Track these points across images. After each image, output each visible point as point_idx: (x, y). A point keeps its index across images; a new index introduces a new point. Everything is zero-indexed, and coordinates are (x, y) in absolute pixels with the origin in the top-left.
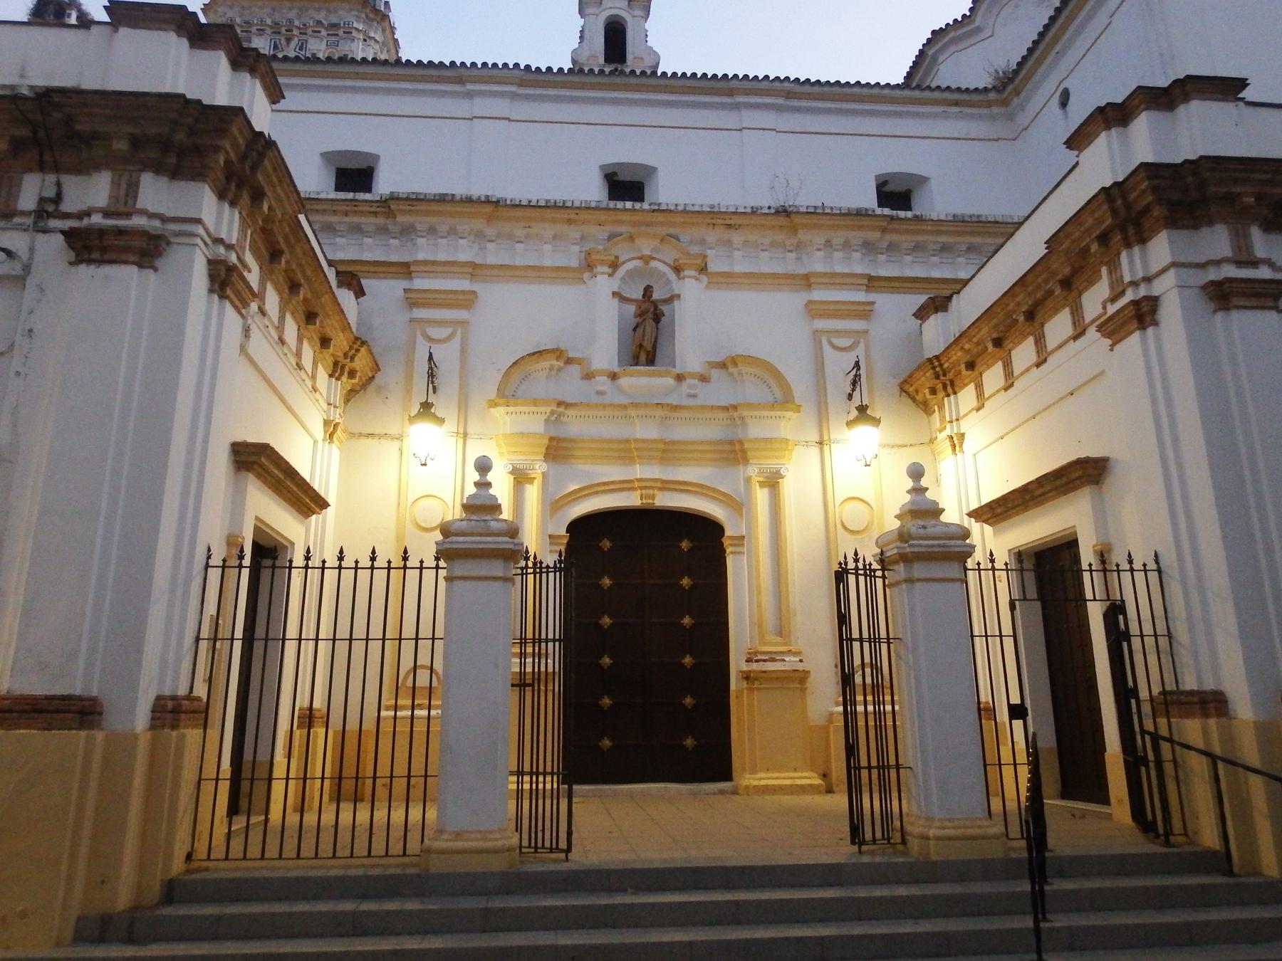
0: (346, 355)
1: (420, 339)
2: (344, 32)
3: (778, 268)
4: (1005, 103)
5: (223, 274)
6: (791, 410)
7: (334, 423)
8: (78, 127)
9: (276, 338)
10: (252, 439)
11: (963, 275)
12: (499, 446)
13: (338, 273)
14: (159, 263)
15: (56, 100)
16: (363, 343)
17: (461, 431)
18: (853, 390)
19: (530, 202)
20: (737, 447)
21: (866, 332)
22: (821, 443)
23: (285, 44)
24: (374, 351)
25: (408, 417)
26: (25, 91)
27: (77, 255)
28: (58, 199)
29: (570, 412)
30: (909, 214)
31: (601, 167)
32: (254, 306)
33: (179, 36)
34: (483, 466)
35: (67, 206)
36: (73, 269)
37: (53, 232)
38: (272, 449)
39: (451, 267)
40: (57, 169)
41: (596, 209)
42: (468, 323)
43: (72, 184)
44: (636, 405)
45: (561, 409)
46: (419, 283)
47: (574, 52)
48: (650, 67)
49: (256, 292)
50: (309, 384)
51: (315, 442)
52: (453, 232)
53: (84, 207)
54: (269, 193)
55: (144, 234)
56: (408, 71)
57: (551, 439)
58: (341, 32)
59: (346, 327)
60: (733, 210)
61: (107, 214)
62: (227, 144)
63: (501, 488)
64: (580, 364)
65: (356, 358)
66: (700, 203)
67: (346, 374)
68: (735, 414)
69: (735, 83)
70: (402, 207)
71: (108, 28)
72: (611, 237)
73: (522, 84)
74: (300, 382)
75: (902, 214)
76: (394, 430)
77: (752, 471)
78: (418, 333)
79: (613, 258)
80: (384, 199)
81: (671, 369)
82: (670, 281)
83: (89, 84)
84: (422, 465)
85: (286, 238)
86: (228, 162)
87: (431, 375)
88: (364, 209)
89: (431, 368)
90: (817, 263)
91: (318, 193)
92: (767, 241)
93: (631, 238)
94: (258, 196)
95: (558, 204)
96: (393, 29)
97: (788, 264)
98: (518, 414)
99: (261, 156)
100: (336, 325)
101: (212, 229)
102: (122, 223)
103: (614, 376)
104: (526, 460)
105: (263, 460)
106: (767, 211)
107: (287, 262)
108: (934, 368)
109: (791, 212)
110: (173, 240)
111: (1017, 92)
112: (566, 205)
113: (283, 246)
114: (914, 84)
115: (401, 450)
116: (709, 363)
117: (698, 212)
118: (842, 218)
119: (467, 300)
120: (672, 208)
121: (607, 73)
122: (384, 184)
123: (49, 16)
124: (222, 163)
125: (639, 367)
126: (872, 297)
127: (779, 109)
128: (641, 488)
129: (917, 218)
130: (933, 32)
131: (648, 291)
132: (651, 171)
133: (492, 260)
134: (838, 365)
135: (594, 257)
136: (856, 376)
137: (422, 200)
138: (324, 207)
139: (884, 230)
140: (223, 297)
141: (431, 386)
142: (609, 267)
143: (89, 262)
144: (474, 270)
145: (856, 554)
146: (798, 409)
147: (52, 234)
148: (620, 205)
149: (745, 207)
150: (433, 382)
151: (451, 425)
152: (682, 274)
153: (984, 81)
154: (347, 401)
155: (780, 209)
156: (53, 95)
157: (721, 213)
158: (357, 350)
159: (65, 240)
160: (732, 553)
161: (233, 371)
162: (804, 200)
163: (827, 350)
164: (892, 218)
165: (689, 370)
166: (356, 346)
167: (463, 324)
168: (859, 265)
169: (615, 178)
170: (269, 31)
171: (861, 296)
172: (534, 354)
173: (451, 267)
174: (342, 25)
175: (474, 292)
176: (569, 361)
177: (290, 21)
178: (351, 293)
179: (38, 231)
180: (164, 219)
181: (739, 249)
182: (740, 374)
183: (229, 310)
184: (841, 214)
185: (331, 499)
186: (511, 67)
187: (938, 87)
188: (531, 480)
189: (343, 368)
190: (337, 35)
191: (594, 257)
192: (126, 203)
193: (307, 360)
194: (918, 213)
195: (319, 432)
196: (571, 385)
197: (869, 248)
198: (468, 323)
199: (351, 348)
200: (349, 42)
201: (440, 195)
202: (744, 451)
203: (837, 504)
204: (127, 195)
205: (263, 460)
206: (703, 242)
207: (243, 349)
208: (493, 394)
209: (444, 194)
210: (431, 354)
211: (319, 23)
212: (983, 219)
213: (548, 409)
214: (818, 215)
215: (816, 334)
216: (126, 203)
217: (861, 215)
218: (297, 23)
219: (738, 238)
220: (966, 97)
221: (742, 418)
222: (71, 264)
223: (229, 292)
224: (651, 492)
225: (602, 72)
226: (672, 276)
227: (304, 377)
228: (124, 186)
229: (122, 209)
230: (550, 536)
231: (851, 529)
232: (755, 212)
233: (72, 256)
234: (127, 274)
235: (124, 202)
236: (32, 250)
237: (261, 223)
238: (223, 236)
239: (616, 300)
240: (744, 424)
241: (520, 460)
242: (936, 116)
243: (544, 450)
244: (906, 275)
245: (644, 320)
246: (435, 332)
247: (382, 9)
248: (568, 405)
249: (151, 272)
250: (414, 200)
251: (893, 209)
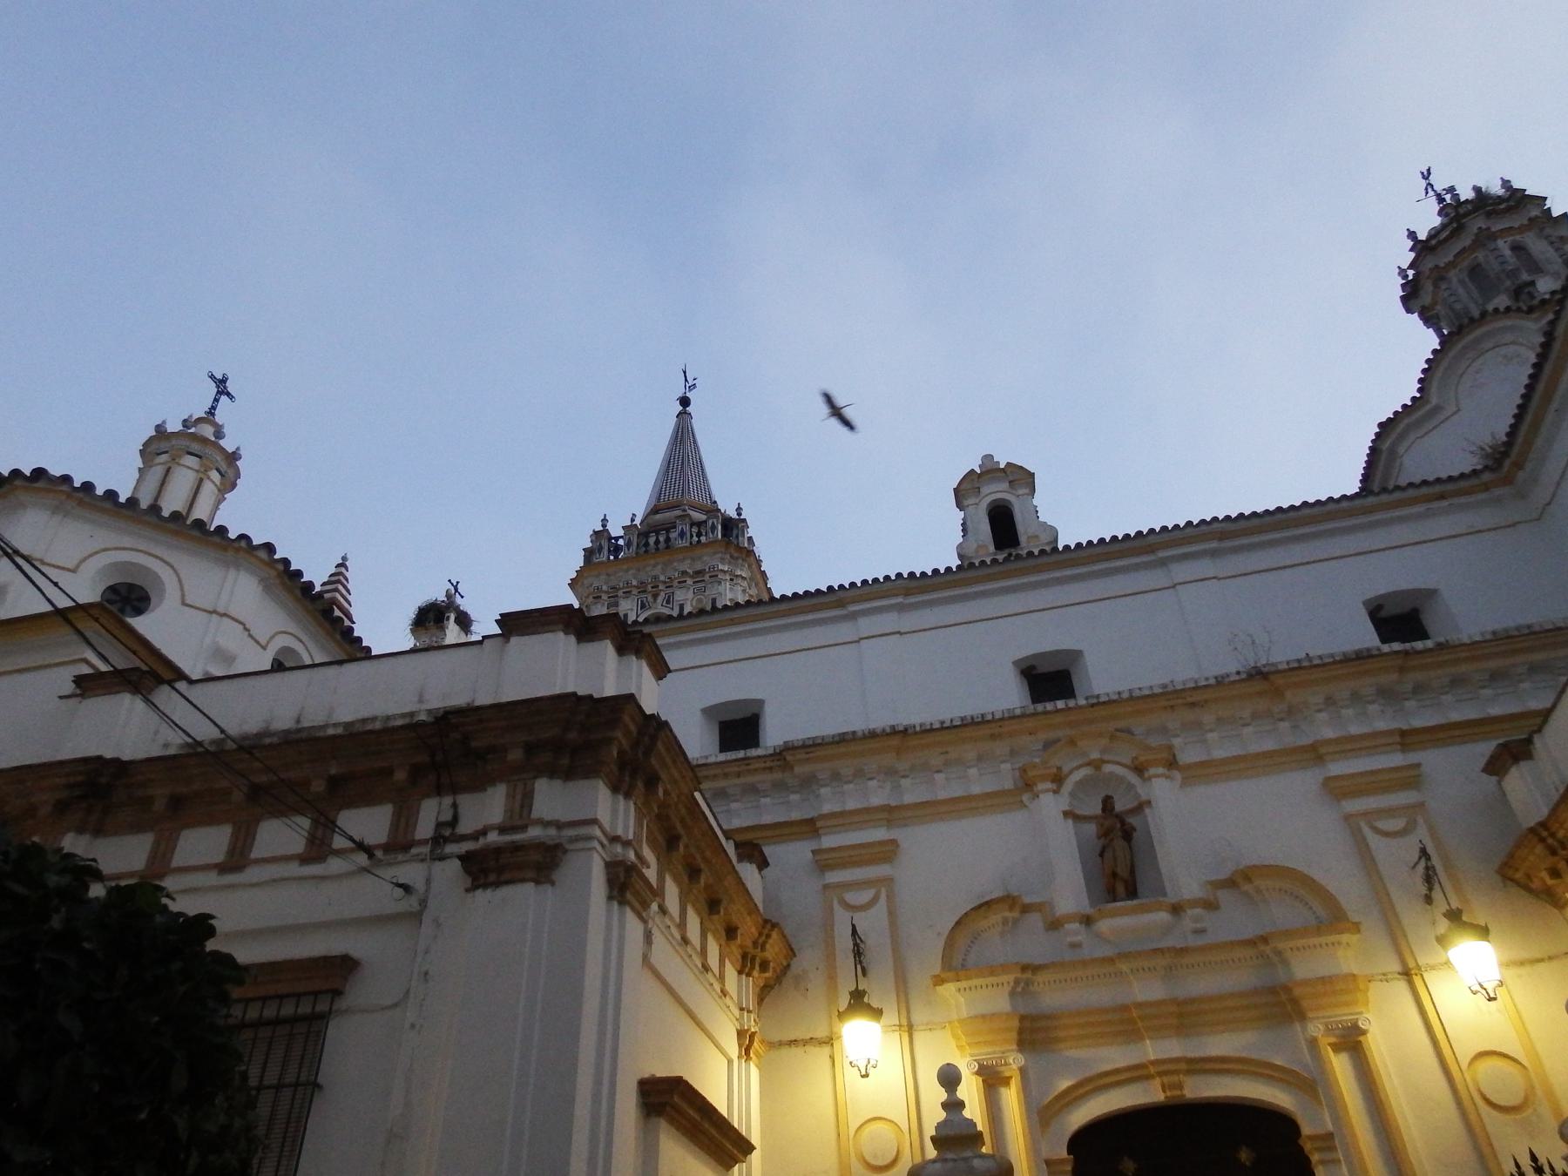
0: (755, 943)
1: (839, 911)
2: (710, 577)
3: (1269, 745)
4: (1508, 481)
5: (622, 875)
6: (1348, 930)
7: (750, 1033)
8: (474, 744)
9: (679, 937)
10: (661, 1072)
11: (1535, 704)
12: (955, 1036)
13: (737, 846)
14: (555, 876)
15: (454, 721)
16: (774, 926)
17: (904, 1022)
18: (1430, 889)
19: (942, 723)
20: (1284, 997)
21: (1422, 805)
22: (1407, 974)
23: (652, 600)
24: (786, 932)
25: (837, 1014)
26: (423, 717)
27: (473, 880)
28: (455, 821)
29: (1041, 978)
30: (1429, 644)
31: (1016, 663)
32: (654, 907)
33: (566, 634)
34: (949, 1078)
35: (464, 828)
36: (471, 895)
37: (449, 858)
38: (687, 1083)
39: (865, 816)
40: (455, 789)
41: (1023, 716)
42: (892, 879)
43: (466, 802)
44: (1124, 956)
45: (1028, 975)
46: (828, 841)
47: (960, 547)
48: (1048, 544)
49: (655, 887)
50: (717, 987)
51: (730, 1062)
52: (859, 774)
53: (480, 826)
54: (663, 776)
55: (540, 846)
56: (784, 606)
57: (1023, 1018)
58: (707, 577)
59: (753, 909)
60: (1192, 685)
61: (503, 830)
62: (619, 734)
63: (974, 1111)
64: (1040, 911)
65: (768, 946)
66: (1149, 684)
67: (757, 967)
68: (1267, 949)
69: (1152, 538)
70: (798, 757)
71: (500, 639)
72: (1048, 745)
73: (908, 593)
74: (708, 987)
75: (1419, 645)
76: (821, 1033)
77: (1316, 1029)
78: (835, 902)
79: (1055, 770)
80: (778, 751)
81: (1161, 899)
82: (1133, 785)
83: (484, 699)
84: (862, 1076)
85: (682, 821)
86: (621, 752)
87: (858, 953)
88: (757, 766)
89: (856, 945)
90: (1324, 729)
91: (707, 757)
92: (1246, 714)
93: (1072, 742)
94: (652, 781)
95: (976, 720)
96: (759, 562)
97: (1284, 736)
98: (979, 988)
99: (654, 739)
100: (742, 909)
101: (607, 827)
102: (518, 837)
103: (1087, 921)
104: (994, 1053)
105: (676, 1099)
106: (1237, 678)
107: (686, 847)
108: (1543, 840)
109: (1268, 673)
110: (568, 847)
111: (1519, 465)
112: (986, 719)
113: (680, 829)
114: (1376, 488)
115: (832, 1058)
116: (1211, 883)
117: (1148, 696)
118: (1339, 666)
119: (887, 852)
120: (1115, 697)
121: (1001, 561)
122: (774, 734)
123: (429, 622)
124: (615, 755)
125: (1118, 904)
126: (1412, 758)
127: (1214, 554)
128: (1161, 1074)
129: (1441, 647)
130: (1381, 425)
131: (1107, 803)
132: (1075, 656)
133: (908, 799)
134: (1396, 856)
135: (1030, 774)
136: (1427, 868)
137: (819, 744)
138: (712, 772)
139: (1402, 670)
140: (622, 903)
141: (859, 967)
142: (1053, 781)
143: (485, 886)
144: (891, 814)
145: (1534, 1158)
146: (1356, 928)
147: (449, 860)
148: (1049, 706)
149: (1207, 679)
150: (861, 962)
151: (891, 1017)
152: (1146, 775)
153: (1466, 463)
154: (761, 1000)
155: (1254, 673)
156: (450, 716)
157: (1176, 691)
158: (768, 936)
159: (462, 864)
160: (1323, 1162)
161: (641, 994)
162: (1281, 655)
163: (1373, 840)
164: (1406, 653)
165: (1186, 897)
166: (766, 931)
167: (888, 881)
168: (1383, 720)
169: (1034, 672)
170: (635, 592)
171: (1397, 759)
172: (980, 906)
173: (865, 816)
174: (707, 570)
175: (894, 842)
176: (1026, 909)
177: (656, 577)
178: (754, 867)
179: (434, 859)
180: (560, 825)
181: (1211, 731)
182: (1258, 891)
183: (630, 915)
184: (1335, 662)
185: (755, 1139)
186: (893, 578)
187: (1411, 485)
188: (1006, 1082)
189: (753, 959)
190: (704, 581)
191: (1030, 774)
192: (521, 816)
193: (713, 960)
194: (1442, 639)
195: (733, 1048)
196: (1033, 942)
197: (1387, 695)
198: (892, 879)
199: (760, 934)
200: (716, 585)
201: (839, 735)
202: (1295, 1001)
203: (1464, 1066)
204: (522, 807)
205: (676, 1099)
206: (1164, 730)
207: (646, 959)
208: (937, 969)
209: (844, 733)
210: (854, 926)
211: (684, 573)
212: (1537, 628)
213: (1010, 978)
214: (1307, 670)
215: (1347, 818)
216: (521, 816)
217: (1363, 658)
218: (662, 578)
219: (1208, 718)
220: (1450, 487)
221: (1279, 953)
222: (467, 890)
223: (629, 896)
224: (1175, 1078)
225: (994, 561)
226: (1133, 778)
227: (712, 980)
228: (519, 797)
229: (519, 823)
230: (1048, 1163)
231: (1502, 1103)
232: (1220, 681)
233: (469, 881)
234: (524, 893)
235: (519, 816)
236: (428, 881)
237: (656, 810)
238: (620, 832)
239: (1070, 822)
240: (1285, 963)
241: (987, 1053)
242: (1419, 517)
243: (1014, 1035)
244: (1453, 720)
245: (1112, 840)
246: (853, 898)
247: (746, 545)
248: (1036, 969)
249: (548, 888)
250: (811, 747)
251: (1404, 642)
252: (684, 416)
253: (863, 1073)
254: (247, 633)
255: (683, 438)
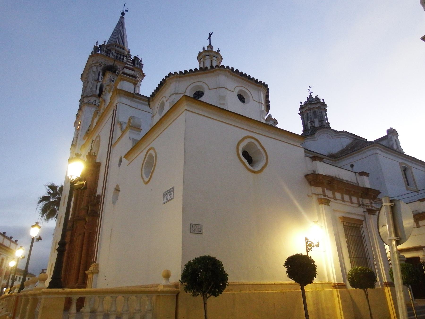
252: (122, 18)
253: (95, 101)
254: (226, 88)
255: (121, 25)
